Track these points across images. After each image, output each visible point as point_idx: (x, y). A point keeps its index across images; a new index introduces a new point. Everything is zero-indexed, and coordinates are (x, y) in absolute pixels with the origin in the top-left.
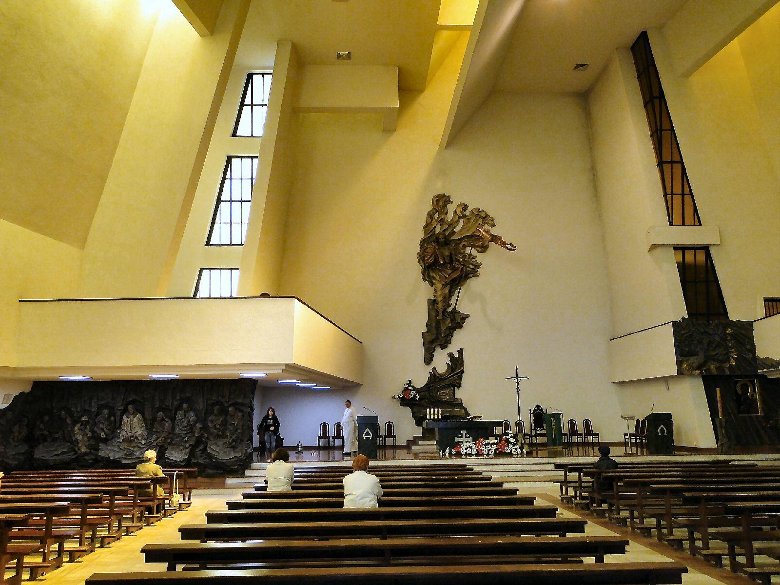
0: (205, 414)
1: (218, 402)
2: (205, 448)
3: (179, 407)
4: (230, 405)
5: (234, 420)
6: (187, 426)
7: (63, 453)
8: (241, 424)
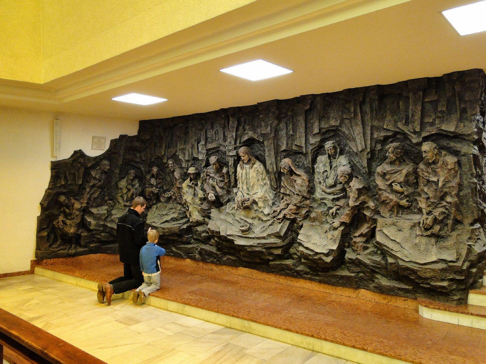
0: (370, 161)
1: (396, 133)
2: (371, 234)
3: (319, 150)
4: (426, 139)
5: (436, 173)
6: (334, 186)
7: (173, 219)
8: (454, 182)
